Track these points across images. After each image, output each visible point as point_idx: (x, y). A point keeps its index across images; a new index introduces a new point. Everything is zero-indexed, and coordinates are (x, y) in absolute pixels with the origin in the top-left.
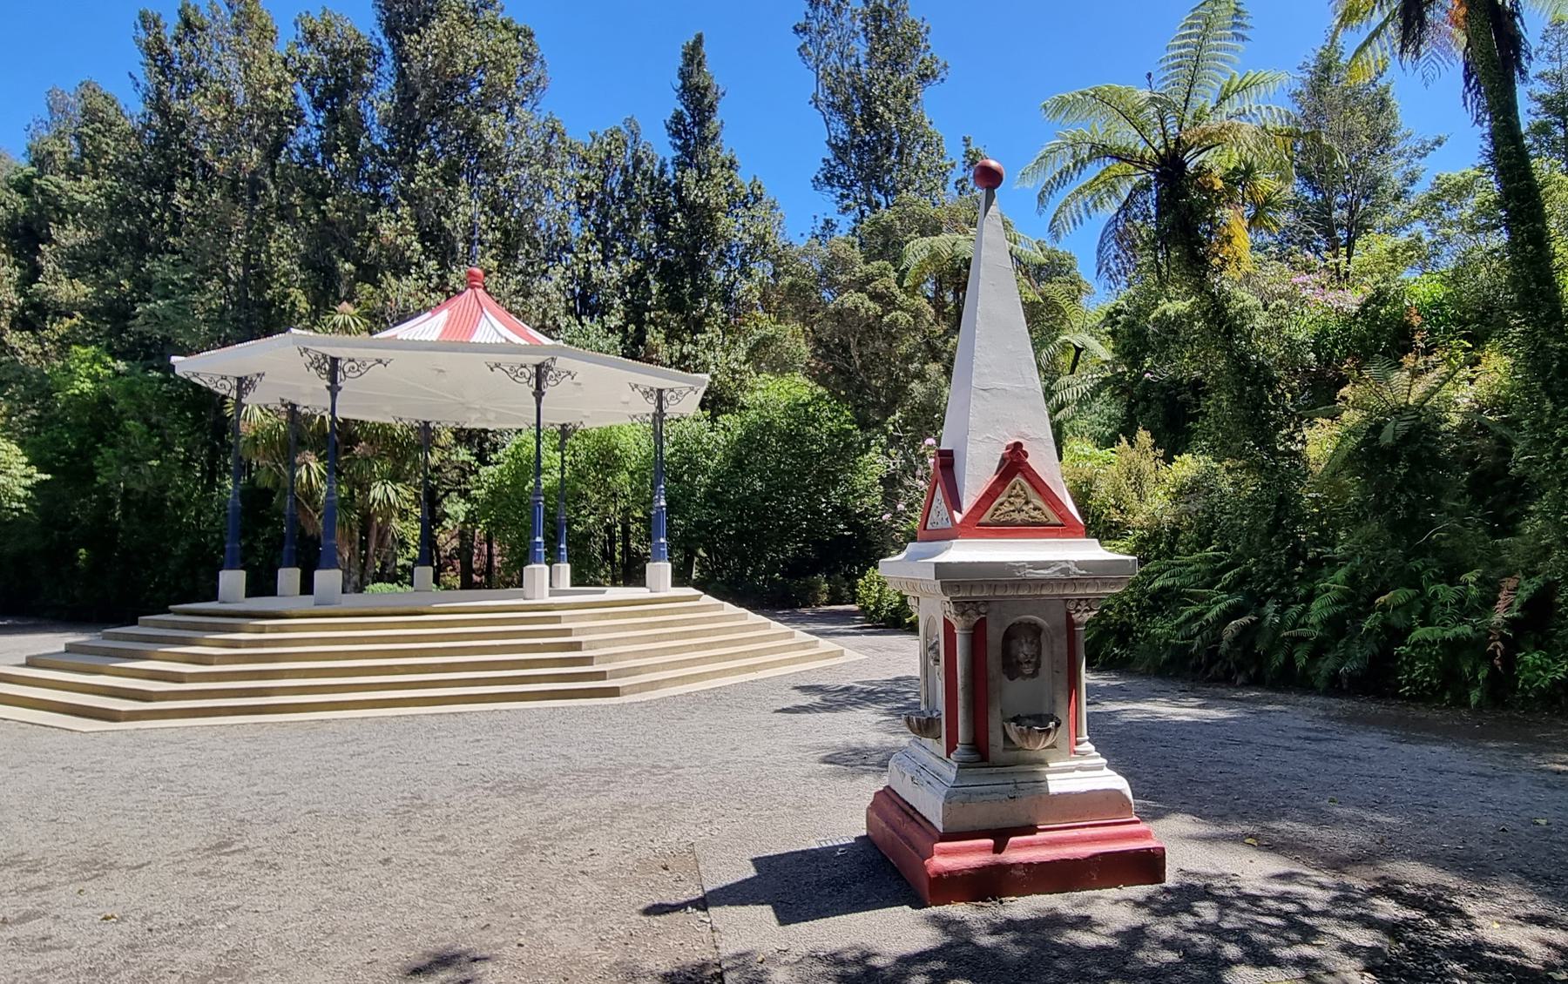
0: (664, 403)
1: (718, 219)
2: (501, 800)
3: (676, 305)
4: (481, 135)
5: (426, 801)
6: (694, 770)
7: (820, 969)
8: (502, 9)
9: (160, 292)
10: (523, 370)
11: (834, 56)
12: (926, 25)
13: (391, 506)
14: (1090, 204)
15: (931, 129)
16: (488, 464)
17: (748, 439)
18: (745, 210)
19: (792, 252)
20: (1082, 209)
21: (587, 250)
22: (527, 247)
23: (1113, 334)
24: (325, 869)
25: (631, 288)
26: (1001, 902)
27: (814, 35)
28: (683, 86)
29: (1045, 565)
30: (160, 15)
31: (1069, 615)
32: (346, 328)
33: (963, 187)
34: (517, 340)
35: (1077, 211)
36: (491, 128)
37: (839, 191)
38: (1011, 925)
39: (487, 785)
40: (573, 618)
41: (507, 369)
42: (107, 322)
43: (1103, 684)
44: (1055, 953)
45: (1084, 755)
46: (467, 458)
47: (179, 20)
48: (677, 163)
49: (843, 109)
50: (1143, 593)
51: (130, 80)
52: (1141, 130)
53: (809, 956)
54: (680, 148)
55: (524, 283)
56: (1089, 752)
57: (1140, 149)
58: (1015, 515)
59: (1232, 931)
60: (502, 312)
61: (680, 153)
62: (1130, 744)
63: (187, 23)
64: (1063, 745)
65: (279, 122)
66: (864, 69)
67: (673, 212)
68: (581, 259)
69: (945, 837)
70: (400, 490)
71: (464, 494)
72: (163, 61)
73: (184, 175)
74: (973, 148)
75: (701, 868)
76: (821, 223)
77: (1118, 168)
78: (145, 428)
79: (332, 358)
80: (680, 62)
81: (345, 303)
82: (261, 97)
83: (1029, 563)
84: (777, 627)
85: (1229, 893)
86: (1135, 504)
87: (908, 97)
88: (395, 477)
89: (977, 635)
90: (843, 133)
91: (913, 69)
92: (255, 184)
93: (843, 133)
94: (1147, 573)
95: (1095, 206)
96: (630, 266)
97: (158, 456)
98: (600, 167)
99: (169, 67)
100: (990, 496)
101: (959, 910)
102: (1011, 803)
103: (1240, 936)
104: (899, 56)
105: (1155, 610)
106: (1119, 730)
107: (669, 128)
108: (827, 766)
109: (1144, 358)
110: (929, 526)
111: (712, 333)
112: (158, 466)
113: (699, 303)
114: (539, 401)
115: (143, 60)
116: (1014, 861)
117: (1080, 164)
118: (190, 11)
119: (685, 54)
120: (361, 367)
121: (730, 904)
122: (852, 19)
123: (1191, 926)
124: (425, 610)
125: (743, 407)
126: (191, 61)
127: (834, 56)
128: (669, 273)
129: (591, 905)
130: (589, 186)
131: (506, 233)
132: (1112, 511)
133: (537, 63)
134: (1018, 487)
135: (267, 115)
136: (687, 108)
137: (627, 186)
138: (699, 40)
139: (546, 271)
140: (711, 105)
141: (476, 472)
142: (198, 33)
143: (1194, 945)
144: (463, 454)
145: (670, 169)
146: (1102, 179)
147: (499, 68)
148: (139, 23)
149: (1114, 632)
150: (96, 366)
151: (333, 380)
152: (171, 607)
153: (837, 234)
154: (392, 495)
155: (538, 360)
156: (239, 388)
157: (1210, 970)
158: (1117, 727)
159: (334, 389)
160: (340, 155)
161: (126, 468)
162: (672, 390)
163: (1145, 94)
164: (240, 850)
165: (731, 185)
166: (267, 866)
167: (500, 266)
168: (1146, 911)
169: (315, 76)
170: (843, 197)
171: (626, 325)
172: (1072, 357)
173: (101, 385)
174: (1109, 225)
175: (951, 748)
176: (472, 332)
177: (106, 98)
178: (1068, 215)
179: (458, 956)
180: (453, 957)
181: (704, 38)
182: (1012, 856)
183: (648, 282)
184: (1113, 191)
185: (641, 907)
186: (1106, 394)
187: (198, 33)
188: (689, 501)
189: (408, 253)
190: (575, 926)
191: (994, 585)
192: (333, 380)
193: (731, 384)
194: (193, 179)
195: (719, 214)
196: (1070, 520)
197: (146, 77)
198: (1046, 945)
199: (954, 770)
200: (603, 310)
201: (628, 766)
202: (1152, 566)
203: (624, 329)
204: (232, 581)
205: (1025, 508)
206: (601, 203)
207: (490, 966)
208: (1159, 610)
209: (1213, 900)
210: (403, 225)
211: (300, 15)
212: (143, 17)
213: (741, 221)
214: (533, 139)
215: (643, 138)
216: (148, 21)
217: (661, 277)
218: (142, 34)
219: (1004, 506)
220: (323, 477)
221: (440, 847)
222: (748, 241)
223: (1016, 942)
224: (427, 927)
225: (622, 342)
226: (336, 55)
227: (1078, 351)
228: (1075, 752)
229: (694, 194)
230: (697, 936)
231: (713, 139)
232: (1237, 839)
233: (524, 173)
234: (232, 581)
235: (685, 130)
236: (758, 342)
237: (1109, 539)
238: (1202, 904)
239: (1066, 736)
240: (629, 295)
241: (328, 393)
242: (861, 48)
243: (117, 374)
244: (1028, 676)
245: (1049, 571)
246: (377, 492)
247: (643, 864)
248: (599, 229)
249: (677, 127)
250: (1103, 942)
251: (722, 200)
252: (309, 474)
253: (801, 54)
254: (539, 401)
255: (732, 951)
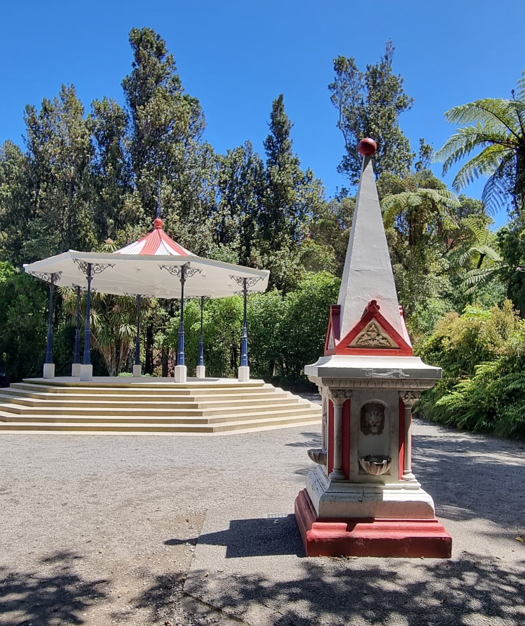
0: (247, 285)
1: (289, 191)
2: (131, 480)
3: (267, 236)
4: (172, 154)
5: (98, 477)
6: (229, 472)
7: (234, 584)
8: (183, 90)
9: (33, 236)
10: (176, 268)
11: (350, 100)
12: (401, 78)
13: (129, 336)
14: (478, 171)
15: (402, 135)
16: (174, 316)
17: (300, 305)
18: (302, 185)
19: (324, 207)
20: (473, 173)
21: (223, 209)
22: (194, 209)
23: (501, 245)
24: (37, 505)
25: (244, 228)
26: (348, 559)
27: (339, 89)
28: (273, 123)
29: (384, 371)
30: (34, 106)
31: (401, 401)
32: (110, 250)
33: (419, 167)
34: (175, 253)
35: (470, 174)
36: (177, 150)
37: (351, 172)
38: (349, 572)
39: (129, 471)
40: (196, 393)
41: (168, 268)
42: (13, 250)
43: (474, 441)
44: (365, 592)
45: (407, 480)
46: (164, 313)
47: (42, 108)
48: (269, 162)
49: (353, 128)
50: (502, 391)
51: (22, 138)
52: (507, 123)
53: (232, 576)
54: (270, 155)
55: (192, 227)
56: (411, 479)
57: (507, 135)
58: (371, 342)
59: (481, 592)
60: (171, 241)
61: (270, 158)
62: (473, 476)
63: (45, 109)
64: (395, 474)
65: (84, 154)
66: (366, 105)
67: (266, 188)
68: (220, 214)
69: (318, 520)
70: (133, 328)
71: (164, 331)
72: (35, 128)
73: (44, 181)
74: (425, 145)
75: (205, 522)
76: (340, 190)
77: (495, 147)
78: (27, 298)
79: (88, 264)
80: (271, 110)
81: (109, 239)
82: (75, 142)
83: (374, 369)
84: (306, 401)
85: (489, 569)
86: (500, 340)
87: (389, 118)
88: (131, 322)
89: (345, 408)
90: (354, 141)
91: (393, 103)
92: (73, 183)
93: (354, 141)
94: (507, 381)
95: (481, 171)
96: (244, 216)
97: (32, 311)
98: (231, 167)
99: (38, 130)
100: (356, 331)
101: (323, 561)
102: (360, 504)
103: (485, 596)
104: (385, 97)
105: (509, 401)
106: (470, 468)
107: (265, 145)
108: (298, 475)
109: (519, 259)
110: (329, 348)
111: (285, 250)
112: (32, 316)
113: (278, 235)
114: (183, 284)
115: (27, 128)
116: (358, 537)
117: (469, 146)
118: (47, 103)
119: (274, 106)
120: (102, 268)
121: (207, 544)
122: (360, 79)
123: (456, 586)
124: (128, 385)
125: (300, 288)
126: (46, 127)
127: (350, 100)
128: (263, 219)
129: (143, 536)
130: (225, 177)
131: (184, 203)
132: (489, 345)
133: (201, 116)
134: (373, 326)
135: (80, 150)
136: (274, 133)
137: (244, 176)
138: (281, 98)
139: (204, 221)
140: (286, 131)
141: (169, 320)
142: (50, 113)
143: (453, 597)
144: (163, 312)
145: (265, 166)
146: (485, 154)
147: (180, 119)
148: (25, 111)
149: (485, 412)
150: (8, 270)
151: (89, 274)
152: (23, 379)
153: (348, 196)
154: (129, 330)
155: (182, 263)
156: (52, 279)
157: (456, 614)
158: (470, 465)
159: (89, 279)
160: (108, 168)
161: (19, 316)
162: (251, 279)
163: (506, 102)
164: (7, 493)
165: (295, 172)
166: (14, 501)
167: (180, 219)
168: (433, 573)
169: (99, 130)
170: (353, 176)
171: (241, 246)
172: (479, 259)
173: (9, 278)
174: (489, 182)
175: (330, 471)
176: (156, 250)
177: (15, 147)
178: (464, 176)
179: (69, 554)
180: (67, 555)
181: (284, 96)
182: (356, 534)
183: (253, 225)
184: (492, 160)
185: (166, 540)
186: (496, 278)
187: (50, 113)
188: (270, 336)
189: (138, 214)
190: (130, 546)
191: (353, 381)
192: (89, 274)
193: (293, 276)
194: (48, 183)
195: (289, 188)
196: (404, 345)
197: (29, 136)
198: (363, 586)
199: (329, 483)
200: (231, 239)
201: (198, 468)
202: (509, 376)
203: (240, 249)
204: (49, 368)
205: (377, 338)
206: (231, 185)
207: (81, 561)
208: (511, 402)
209: (477, 572)
210: (136, 200)
211: (93, 101)
212: (27, 107)
213: (300, 192)
214: (198, 155)
215: (254, 151)
216: (29, 110)
217: (259, 222)
218: (27, 116)
219: (364, 336)
220: (99, 322)
221: (92, 500)
222: (304, 201)
223: (346, 583)
224: (64, 539)
225: (239, 255)
226: (109, 119)
227: (483, 256)
228: (402, 479)
229: (276, 179)
230: (184, 558)
231: (287, 149)
232: (511, 537)
233: (193, 171)
234: (49, 368)
235: (273, 146)
236: (305, 254)
237: (486, 360)
238: (468, 573)
239: (396, 469)
240: (243, 232)
241: (87, 280)
242: (364, 94)
243: (16, 273)
244: (375, 434)
245: (385, 375)
246: (122, 329)
247: (178, 518)
248: (229, 199)
249: (269, 144)
250: (398, 588)
251: (291, 181)
252: (93, 320)
253: (332, 101)
254: (183, 284)
255: (196, 568)
